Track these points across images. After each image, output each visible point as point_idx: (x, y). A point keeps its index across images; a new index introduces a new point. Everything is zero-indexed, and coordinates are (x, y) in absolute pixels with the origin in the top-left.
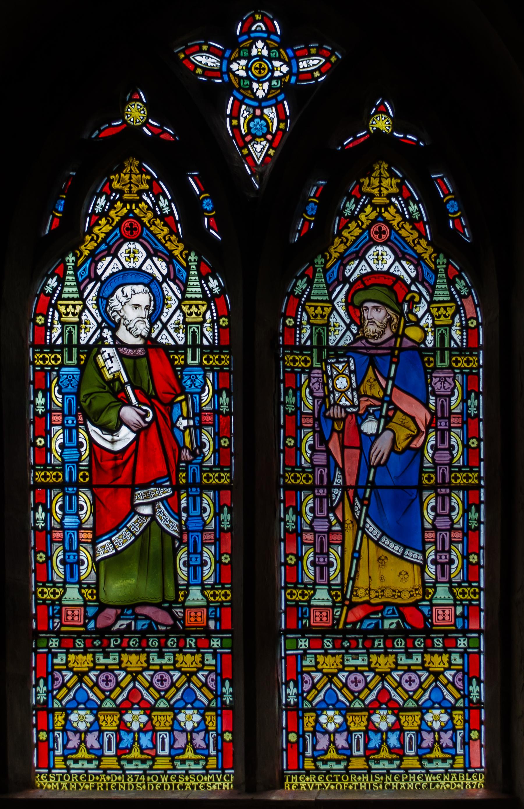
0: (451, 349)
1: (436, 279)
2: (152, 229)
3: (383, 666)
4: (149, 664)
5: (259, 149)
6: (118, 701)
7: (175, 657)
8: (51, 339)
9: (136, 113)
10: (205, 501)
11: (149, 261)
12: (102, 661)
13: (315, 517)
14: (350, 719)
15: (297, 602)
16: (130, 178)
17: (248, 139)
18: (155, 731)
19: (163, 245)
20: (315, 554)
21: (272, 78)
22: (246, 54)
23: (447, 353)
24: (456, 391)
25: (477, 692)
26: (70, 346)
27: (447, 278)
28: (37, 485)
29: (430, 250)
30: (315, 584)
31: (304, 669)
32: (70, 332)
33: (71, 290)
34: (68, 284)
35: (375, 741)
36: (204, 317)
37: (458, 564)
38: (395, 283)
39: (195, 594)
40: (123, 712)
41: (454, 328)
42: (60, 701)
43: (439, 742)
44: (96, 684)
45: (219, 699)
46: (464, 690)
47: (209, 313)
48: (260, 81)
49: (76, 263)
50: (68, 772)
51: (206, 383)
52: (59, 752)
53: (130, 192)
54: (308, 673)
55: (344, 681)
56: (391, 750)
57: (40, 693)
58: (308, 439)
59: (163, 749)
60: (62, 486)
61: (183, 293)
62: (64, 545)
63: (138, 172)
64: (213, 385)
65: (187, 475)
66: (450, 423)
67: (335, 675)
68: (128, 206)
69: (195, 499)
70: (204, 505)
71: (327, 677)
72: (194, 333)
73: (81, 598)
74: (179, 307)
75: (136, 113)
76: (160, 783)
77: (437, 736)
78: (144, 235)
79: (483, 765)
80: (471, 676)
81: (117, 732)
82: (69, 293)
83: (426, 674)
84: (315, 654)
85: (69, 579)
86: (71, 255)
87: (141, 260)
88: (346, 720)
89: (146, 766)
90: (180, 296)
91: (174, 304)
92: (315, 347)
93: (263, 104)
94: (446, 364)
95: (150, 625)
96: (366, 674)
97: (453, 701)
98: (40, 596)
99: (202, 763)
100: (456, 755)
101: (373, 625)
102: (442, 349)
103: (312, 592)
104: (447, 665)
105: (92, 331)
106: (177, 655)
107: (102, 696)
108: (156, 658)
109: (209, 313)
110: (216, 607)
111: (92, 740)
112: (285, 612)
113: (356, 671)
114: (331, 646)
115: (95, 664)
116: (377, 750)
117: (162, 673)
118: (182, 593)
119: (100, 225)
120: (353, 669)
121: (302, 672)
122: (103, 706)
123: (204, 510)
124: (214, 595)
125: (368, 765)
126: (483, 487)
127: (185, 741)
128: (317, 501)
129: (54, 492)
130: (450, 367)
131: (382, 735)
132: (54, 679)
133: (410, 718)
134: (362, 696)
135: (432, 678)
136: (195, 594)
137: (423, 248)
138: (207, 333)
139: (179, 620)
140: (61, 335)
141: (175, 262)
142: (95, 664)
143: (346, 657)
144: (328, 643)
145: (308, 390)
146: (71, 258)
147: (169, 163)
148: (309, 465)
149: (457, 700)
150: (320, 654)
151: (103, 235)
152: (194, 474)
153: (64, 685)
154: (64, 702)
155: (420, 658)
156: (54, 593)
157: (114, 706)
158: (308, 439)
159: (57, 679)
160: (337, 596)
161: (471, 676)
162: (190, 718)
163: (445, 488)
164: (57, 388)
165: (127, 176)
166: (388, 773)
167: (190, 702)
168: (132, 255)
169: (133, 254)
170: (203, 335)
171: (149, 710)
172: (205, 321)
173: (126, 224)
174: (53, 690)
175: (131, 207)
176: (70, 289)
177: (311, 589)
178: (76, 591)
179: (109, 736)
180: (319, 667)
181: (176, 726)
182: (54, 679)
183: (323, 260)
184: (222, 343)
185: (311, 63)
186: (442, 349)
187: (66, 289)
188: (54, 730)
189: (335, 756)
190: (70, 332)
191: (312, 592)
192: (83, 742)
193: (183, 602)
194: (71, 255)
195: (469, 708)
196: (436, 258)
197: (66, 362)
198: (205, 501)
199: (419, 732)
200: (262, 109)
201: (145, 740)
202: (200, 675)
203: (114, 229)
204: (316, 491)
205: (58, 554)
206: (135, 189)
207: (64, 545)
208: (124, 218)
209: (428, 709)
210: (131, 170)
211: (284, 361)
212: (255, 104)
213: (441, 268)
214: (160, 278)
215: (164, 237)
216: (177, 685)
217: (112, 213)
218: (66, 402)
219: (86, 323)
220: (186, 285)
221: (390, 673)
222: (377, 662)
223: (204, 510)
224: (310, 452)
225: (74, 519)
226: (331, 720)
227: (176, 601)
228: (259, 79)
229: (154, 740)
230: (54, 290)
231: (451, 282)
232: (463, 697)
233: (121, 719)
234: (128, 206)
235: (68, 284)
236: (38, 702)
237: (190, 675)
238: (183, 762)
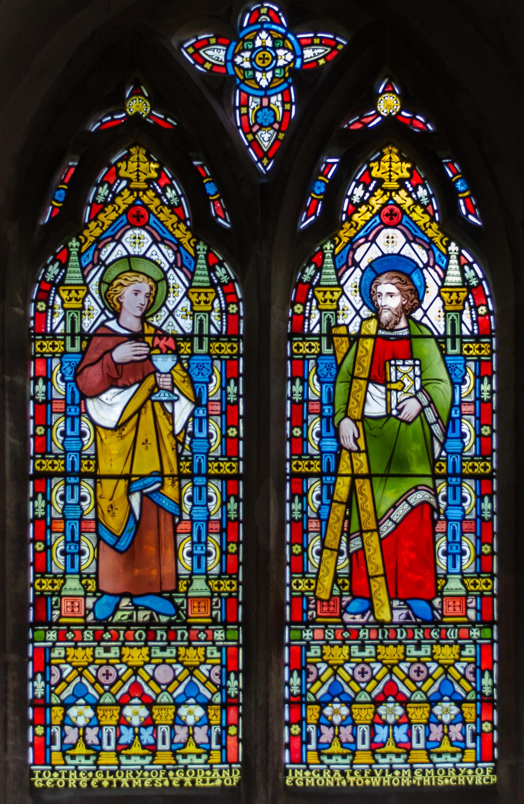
1: (196, 264)
2: (411, 215)
3: (136, 658)
4: (151, 658)
5: (266, 138)
6: (374, 695)
7: (322, 649)
9: (388, 104)
10: (465, 490)
11: (154, 247)
12: (414, 653)
14: (100, 713)
15: (302, 592)
16: (390, 166)
17: (256, 128)
18: (410, 724)
19: (171, 233)
20: (66, 542)
21: (275, 67)
22: (277, 45)
23: (458, 341)
24: (214, 377)
25: (234, 685)
27: (207, 264)
28: (293, 475)
29: (189, 235)
30: (65, 573)
32: (73, 318)
33: (201, 278)
34: (327, 271)
35: (127, 736)
36: (212, 305)
37: (216, 554)
38: (373, 269)
39: (199, 586)
41: (213, 314)
42: (59, 696)
43: (338, 737)
45: (224, 691)
46: (475, 682)
47: (217, 302)
48: (264, 71)
49: (80, 248)
50: (119, 769)
51: (213, 372)
52: (312, 746)
53: (390, 180)
54: (314, 664)
55: (151, 674)
56: (397, 744)
57: (38, 688)
58: (315, 425)
60: (64, 475)
61: (190, 281)
62: (192, 536)
63: (146, 160)
64: (221, 373)
65: (321, 463)
66: (208, 411)
67: (197, 667)
68: (135, 194)
69: (456, 488)
70: (209, 494)
71: (443, 667)
72: (201, 321)
73: (462, 587)
74: (186, 295)
75: (388, 104)
76: (52, 780)
77: (337, 730)
78: (403, 222)
79: (240, 760)
80: (229, 670)
81: (118, 726)
82: (199, 281)
83: (124, 668)
84: (65, 648)
85: (69, 570)
86: (74, 240)
87: (146, 246)
88: (96, 715)
89: (456, 759)
90: (440, 284)
91: (182, 291)
92: (324, 335)
93: (269, 93)
94: (205, 350)
95: (151, 616)
97: (209, 696)
98: (295, 587)
99: (205, 757)
100: (466, 748)
101: (126, 617)
103: (62, 581)
104: (202, 659)
105: (96, 317)
106: (435, 647)
107: (158, 690)
108: (357, 650)
109: (217, 302)
110: (476, 596)
111: (346, 733)
112: (34, 605)
113: (108, 664)
114: (333, 637)
115: (350, 657)
116: (129, 746)
117: (363, 666)
118: (185, 582)
119: (359, 212)
121: (50, 665)
122: (101, 701)
123: (464, 499)
124: (219, 586)
125: (119, 760)
127: (76, 736)
128: (451, 489)
129: (55, 480)
130: (209, 354)
131: (443, 728)
132: (308, 673)
133: (164, 712)
134: (170, 689)
136: (199, 586)
137: (182, 233)
138: (215, 322)
139: (437, 610)
140: (320, 322)
141: (435, 248)
142: (350, 657)
144: (88, 636)
145: (316, 377)
146: (74, 243)
147: (173, 150)
148: (318, 452)
149: (467, 693)
150: (70, 647)
151: (363, 223)
152: (73, 463)
153: (429, 676)
154: (118, 697)
155: (319, 651)
156: (53, 585)
157: (369, 699)
158: (315, 425)
159: (312, 673)
160: (344, 585)
161: (229, 670)
162: (447, 711)
163: (75, 476)
164: (60, 375)
165: (387, 164)
166: (143, 768)
167: (191, 695)
168: (137, 241)
169: (137, 241)
170: (211, 322)
171: (149, 704)
172: (213, 309)
173: (133, 211)
174: (307, 683)
175: (138, 194)
176: (74, 275)
177: (61, 578)
178: (203, 582)
179: (363, 730)
180: (325, 658)
181: (67, 721)
182: (308, 673)
183: (332, 246)
185: (316, 52)
186: (201, 336)
187: (323, 277)
188: (51, 725)
189: (85, 751)
190: (73, 318)
191: (62, 581)
192: (190, 735)
193: (186, 592)
194: (74, 240)
195: (481, 701)
196: (196, 243)
198: (465, 490)
199: (372, 726)
200: (269, 97)
201: (147, 735)
203: (374, 216)
204: (324, 478)
205: (59, 543)
206: (143, 177)
207: (321, 535)
208: (384, 205)
210: (390, 158)
211: (491, 348)
212: (262, 93)
213: (202, 255)
214: (421, 265)
215: (172, 225)
216: (179, 678)
217: (373, 201)
218: (69, 390)
219: (343, 310)
220: (193, 274)
221: (453, 665)
222: (74, 656)
223: (464, 499)
224: (318, 439)
225: (203, 510)
226: (81, 714)
227: (177, 591)
228: (264, 67)
229: (409, 734)
230: (313, 277)
231: (211, 269)
232: (220, 690)
233: (121, 714)
234: (388, 194)
235: (327, 271)
236: (35, 697)
237: (191, 670)
238: (185, 756)
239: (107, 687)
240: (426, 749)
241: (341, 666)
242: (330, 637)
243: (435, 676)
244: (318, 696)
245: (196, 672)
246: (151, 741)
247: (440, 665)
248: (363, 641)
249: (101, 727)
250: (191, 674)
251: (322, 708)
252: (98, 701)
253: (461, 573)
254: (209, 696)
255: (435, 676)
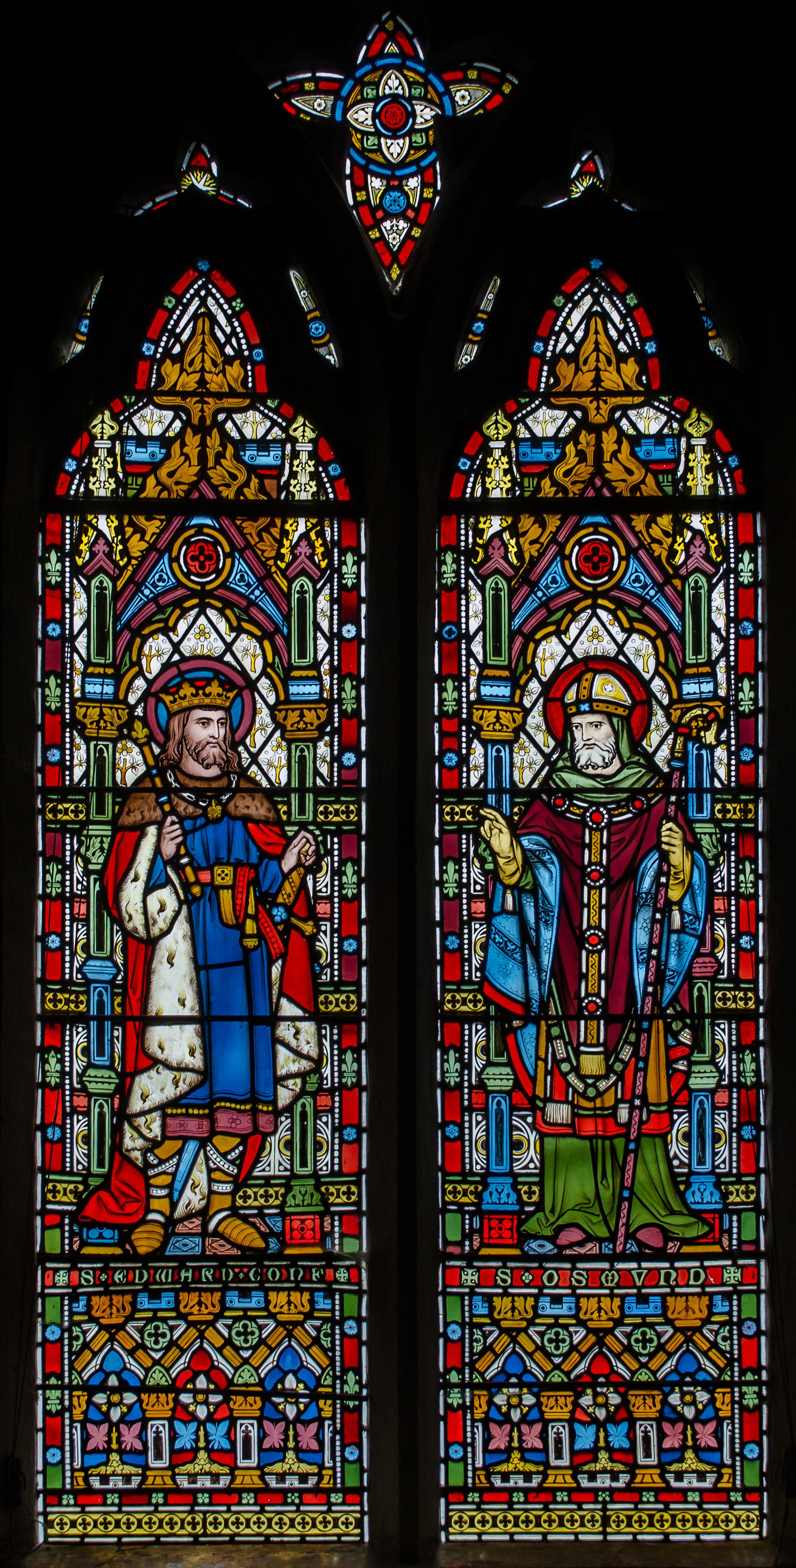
0: (713, 790)
8: (71, 780)
13: (90, 1065)
26: (101, 790)
31: (475, 1320)
40: (494, 1390)
44: (316, 1341)
59: (648, 1455)
96: (659, 1329)
102: (302, 790)
120: (552, 1321)
126: (364, 1019)
134: (653, 1365)
135: (193, 1332)
142: (224, 1308)
143: (183, 1296)
184: (446, 786)
197: (94, 816)
202: (219, 1325)
209: (500, 1386)
239: (557, 1360)
240: (260, 1467)
241: (699, 1330)
242: (579, 1282)
243: (670, 1348)
244: (488, 1375)
245: (120, 1336)
246: (626, 1444)
247: (102, 1327)
248: (226, 1283)
249: (546, 1423)
250: (290, 1335)
251: (491, 1396)
252: (143, 1382)
253: (315, 1175)
254: (715, 1373)
255: (670, 1348)
